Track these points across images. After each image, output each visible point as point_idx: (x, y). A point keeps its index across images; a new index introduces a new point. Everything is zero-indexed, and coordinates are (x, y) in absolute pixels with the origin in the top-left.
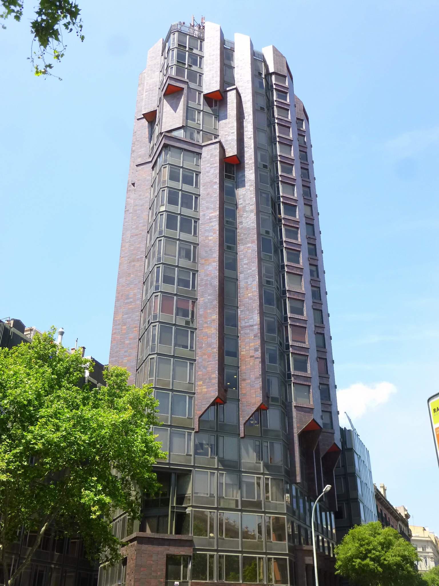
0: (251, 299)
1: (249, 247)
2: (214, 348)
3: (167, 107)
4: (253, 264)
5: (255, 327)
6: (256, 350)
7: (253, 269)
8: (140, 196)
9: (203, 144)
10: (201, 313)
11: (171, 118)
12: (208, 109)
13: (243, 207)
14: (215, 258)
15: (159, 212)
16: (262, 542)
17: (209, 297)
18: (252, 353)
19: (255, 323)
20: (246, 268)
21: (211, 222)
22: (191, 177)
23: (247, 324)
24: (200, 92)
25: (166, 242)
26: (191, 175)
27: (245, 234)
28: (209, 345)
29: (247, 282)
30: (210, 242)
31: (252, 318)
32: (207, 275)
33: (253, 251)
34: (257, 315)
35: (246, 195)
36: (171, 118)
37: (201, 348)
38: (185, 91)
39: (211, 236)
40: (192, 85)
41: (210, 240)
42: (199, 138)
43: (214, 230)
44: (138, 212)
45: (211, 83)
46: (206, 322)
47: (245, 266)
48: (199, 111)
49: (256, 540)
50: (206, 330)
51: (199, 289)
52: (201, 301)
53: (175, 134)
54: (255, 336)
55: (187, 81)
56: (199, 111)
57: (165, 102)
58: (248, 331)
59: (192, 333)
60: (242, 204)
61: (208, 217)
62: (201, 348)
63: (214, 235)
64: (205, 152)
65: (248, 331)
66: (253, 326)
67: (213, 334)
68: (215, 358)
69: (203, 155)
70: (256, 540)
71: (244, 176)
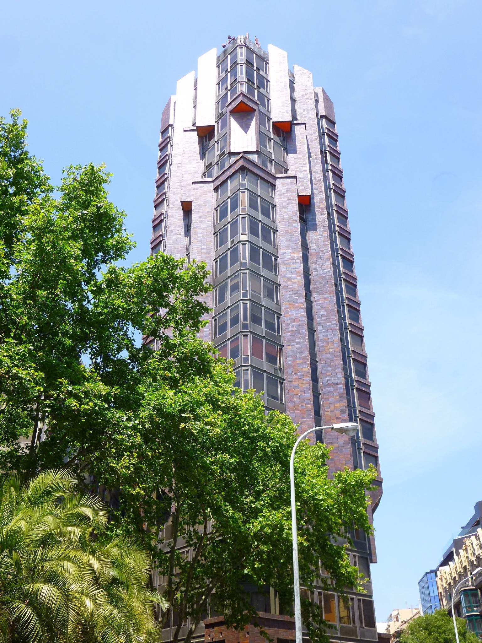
0: (332, 354)
1: (326, 298)
2: (309, 404)
3: (234, 125)
4: (332, 317)
5: (339, 386)
6: (343, 411)
7: (333, 322)
8: (200, 217)
9: (277, 176)
10: (289, 362)
11: (242, 139)
12: (277, 139)
13: (316, 253)
14: (302, 303)
15: (240, 241)
16: (356, 627)
17: (297, 346)
18: (338, 414)
19: (339, 382)
20: (325, 320)
21: (293, 263)
22: (268, 208)
23: (329, 382)
24: (269, 119)
25: (252, 277)
26: (267, 206)
27: (321, 283)
28: (302, 400)
29: (327, 336)
30: (294, 285)
31: (335, 376)
32: (293, 321)
33: (331, 302)
34: (341, 373)
35: (319, 239)
36: (242, 139)
37: (292, 402)
38: (257, 113)
39: (294, 278)
40: (262, 109)
41: (294, 283)
42: (272, 168)
43: (298, 272)
44: (198, 235)
45: (279, 112)
46: (297, 374)
47: (323, 318)
48: (270, 139)
49: (351, 626)
50: (297, 383)
51: (286, 336)
52: (288, 349)
53: (250, 157)
54: (341, 396)
55: (258, 102)
56: (270, 139)
57: (231, 117)
58: (332, 390)
59: (281, 383)
60: (315, 249)
61: (289, 257)
62: (292, 402)
63: (299, 278)
64: (279, 184)
65: (332, 390)
66: (337, 384)
67: (307, 388)
68: (311, 415)
69: (278, 187)
70: (351, 626)
71: (314, 219)
